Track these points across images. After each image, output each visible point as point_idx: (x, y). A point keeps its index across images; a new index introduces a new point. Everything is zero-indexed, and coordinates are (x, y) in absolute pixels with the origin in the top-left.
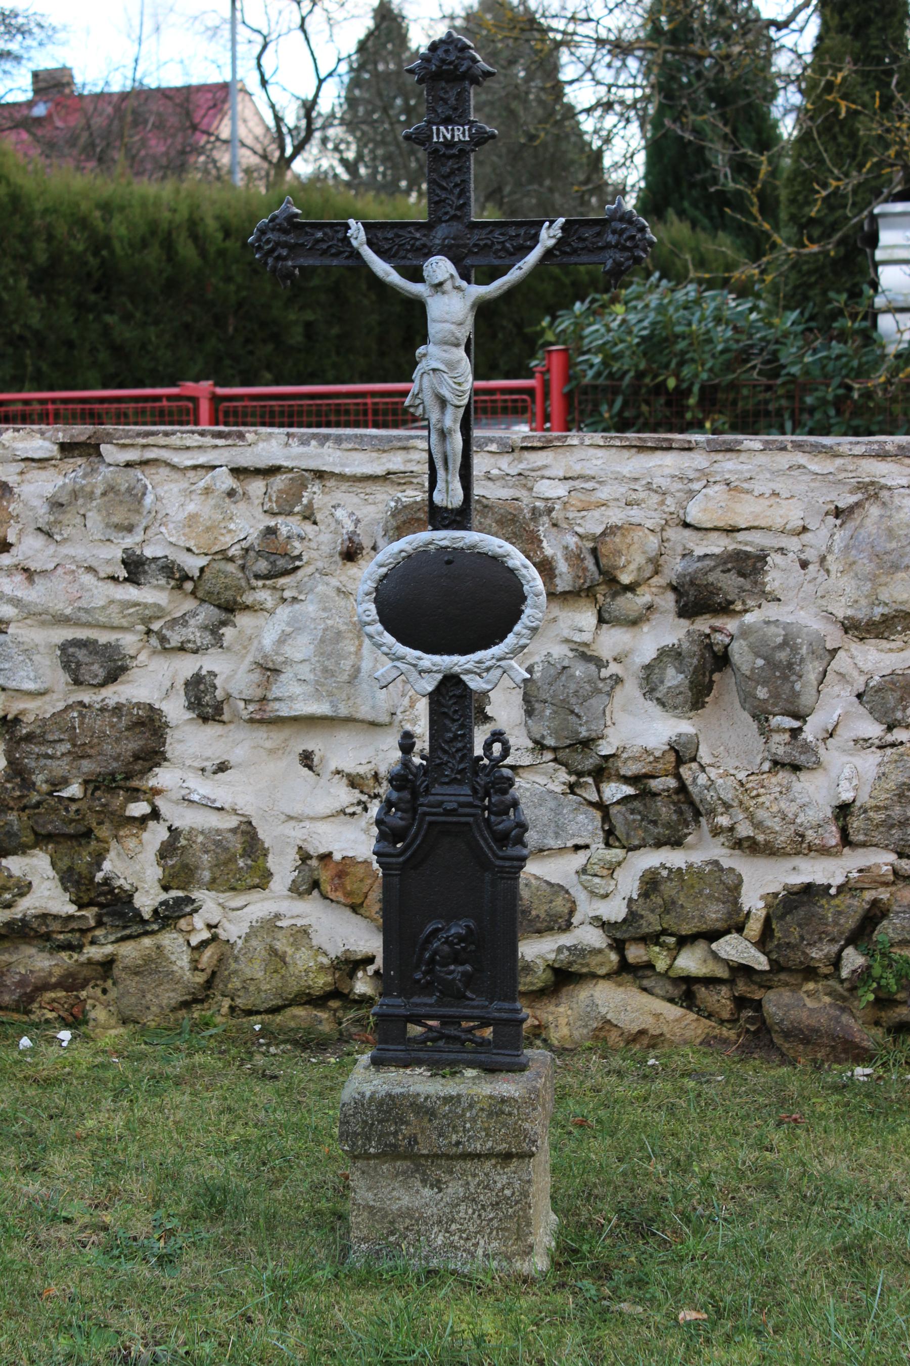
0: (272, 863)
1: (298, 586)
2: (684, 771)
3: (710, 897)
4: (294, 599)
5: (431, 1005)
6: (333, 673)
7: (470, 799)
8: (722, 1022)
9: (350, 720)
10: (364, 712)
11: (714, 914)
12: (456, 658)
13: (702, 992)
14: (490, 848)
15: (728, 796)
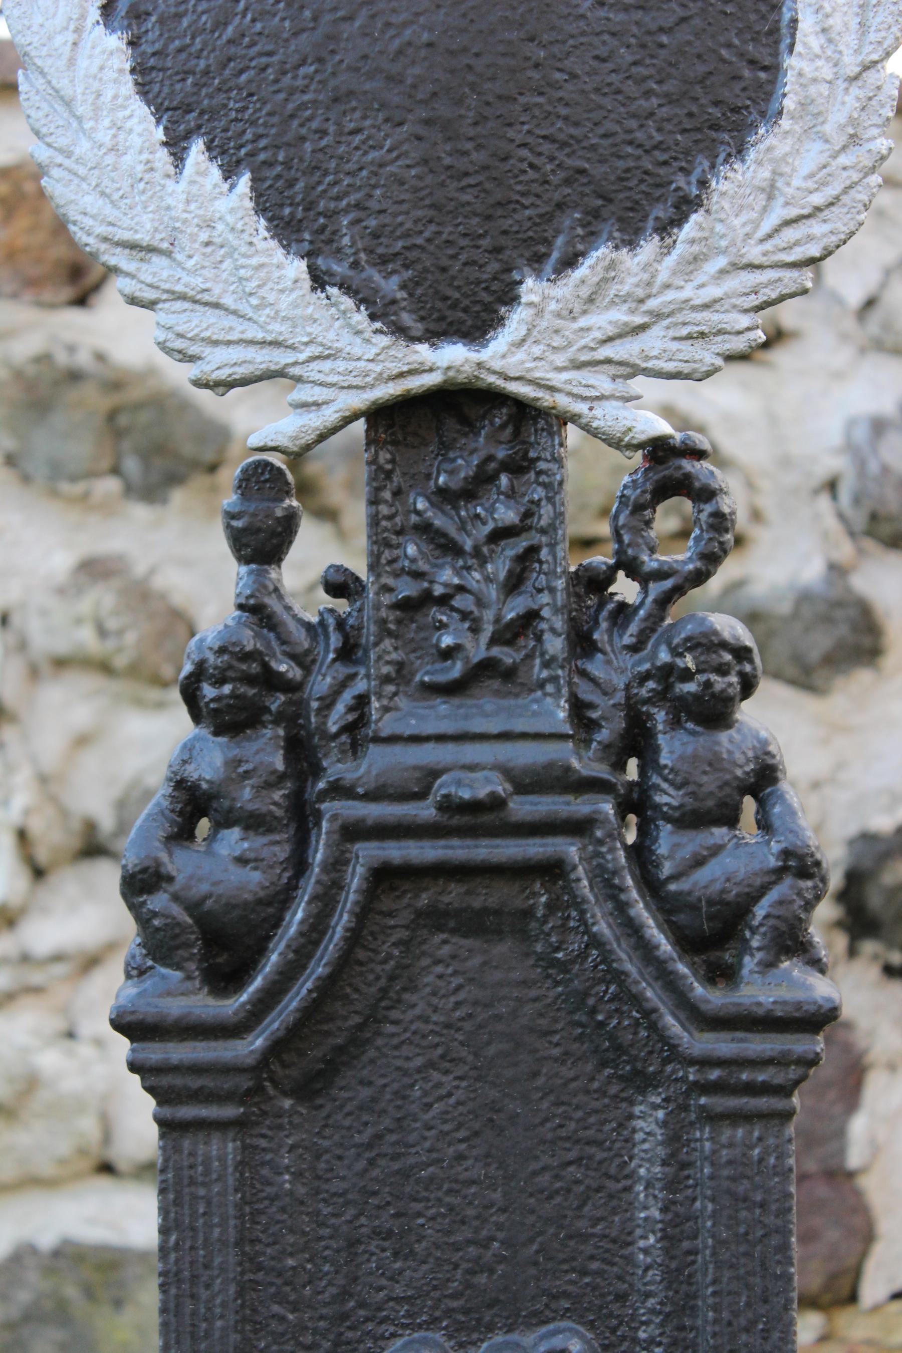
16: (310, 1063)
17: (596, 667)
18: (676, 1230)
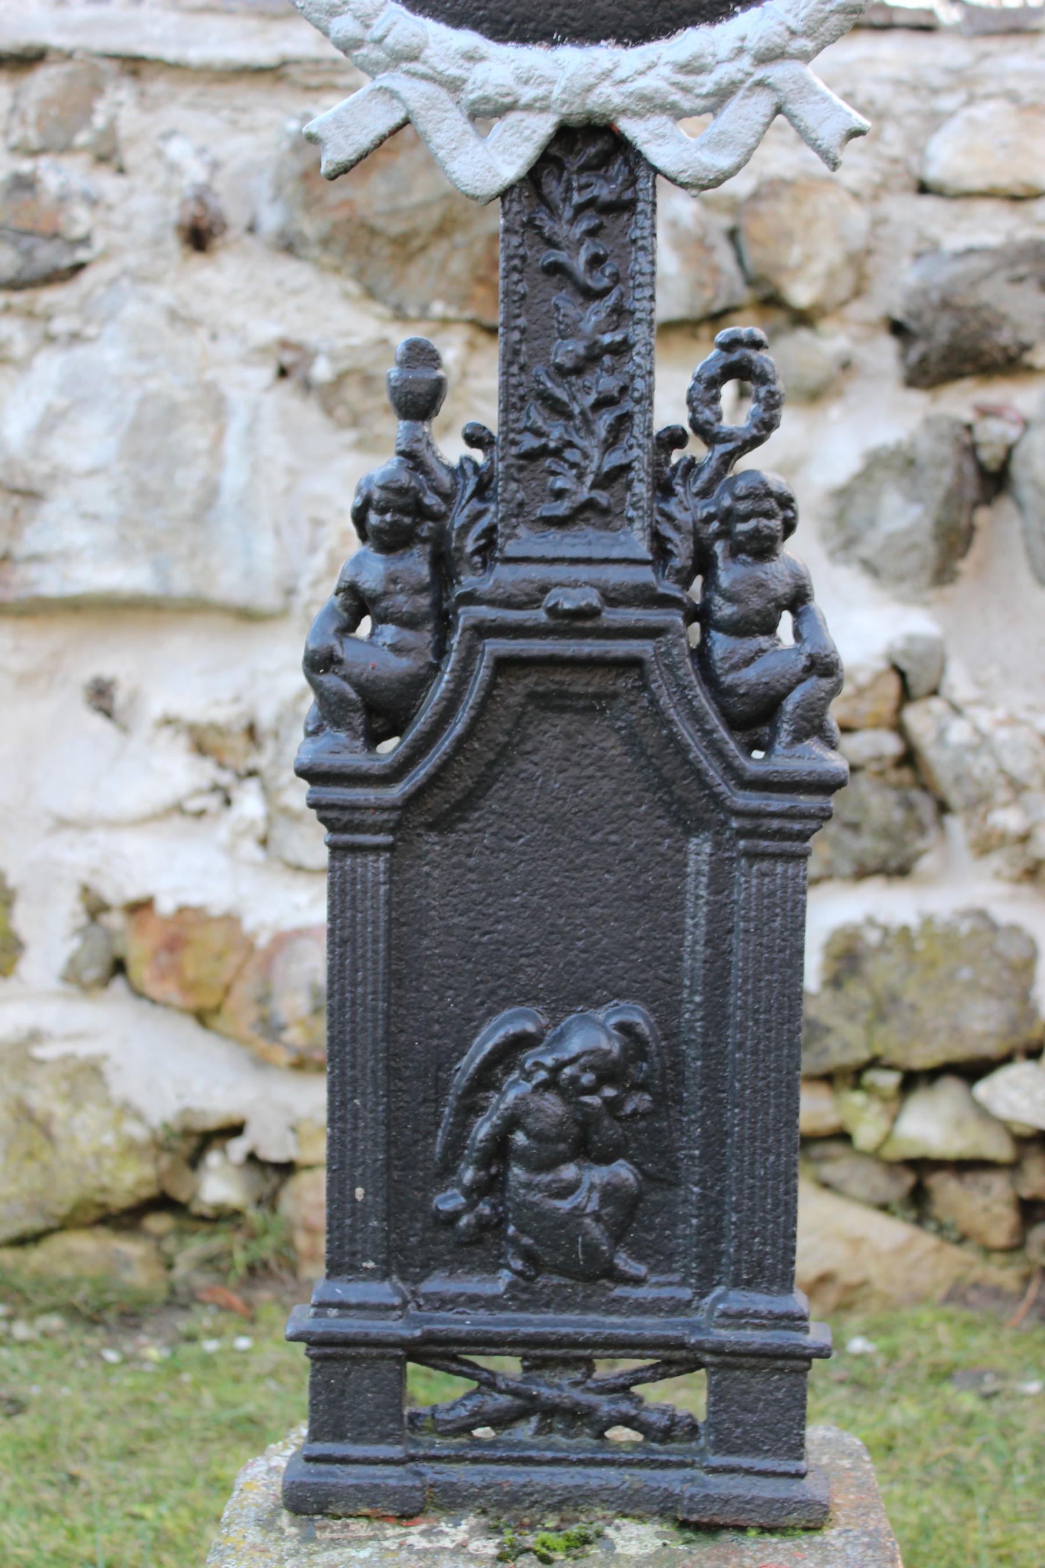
0: (23, 920)
1: (84, 308)
2: (915, 717)
3: (972, 986)
4: (75, 337)
5: (492, 1303)
6: (165, 490)
7: (645, 575)
8: (988, 1251)
9: (194, 608)
10: (228, 584)
11: (981, 1026)
12: (605, 55)
13: (946, 1190)
14: (718, 752)
15: (1019, 765)
16: (438, 807)
17: (672, 507)
18: (717, 938)
